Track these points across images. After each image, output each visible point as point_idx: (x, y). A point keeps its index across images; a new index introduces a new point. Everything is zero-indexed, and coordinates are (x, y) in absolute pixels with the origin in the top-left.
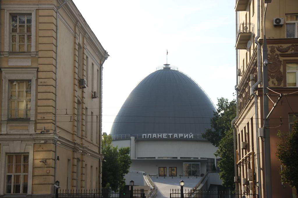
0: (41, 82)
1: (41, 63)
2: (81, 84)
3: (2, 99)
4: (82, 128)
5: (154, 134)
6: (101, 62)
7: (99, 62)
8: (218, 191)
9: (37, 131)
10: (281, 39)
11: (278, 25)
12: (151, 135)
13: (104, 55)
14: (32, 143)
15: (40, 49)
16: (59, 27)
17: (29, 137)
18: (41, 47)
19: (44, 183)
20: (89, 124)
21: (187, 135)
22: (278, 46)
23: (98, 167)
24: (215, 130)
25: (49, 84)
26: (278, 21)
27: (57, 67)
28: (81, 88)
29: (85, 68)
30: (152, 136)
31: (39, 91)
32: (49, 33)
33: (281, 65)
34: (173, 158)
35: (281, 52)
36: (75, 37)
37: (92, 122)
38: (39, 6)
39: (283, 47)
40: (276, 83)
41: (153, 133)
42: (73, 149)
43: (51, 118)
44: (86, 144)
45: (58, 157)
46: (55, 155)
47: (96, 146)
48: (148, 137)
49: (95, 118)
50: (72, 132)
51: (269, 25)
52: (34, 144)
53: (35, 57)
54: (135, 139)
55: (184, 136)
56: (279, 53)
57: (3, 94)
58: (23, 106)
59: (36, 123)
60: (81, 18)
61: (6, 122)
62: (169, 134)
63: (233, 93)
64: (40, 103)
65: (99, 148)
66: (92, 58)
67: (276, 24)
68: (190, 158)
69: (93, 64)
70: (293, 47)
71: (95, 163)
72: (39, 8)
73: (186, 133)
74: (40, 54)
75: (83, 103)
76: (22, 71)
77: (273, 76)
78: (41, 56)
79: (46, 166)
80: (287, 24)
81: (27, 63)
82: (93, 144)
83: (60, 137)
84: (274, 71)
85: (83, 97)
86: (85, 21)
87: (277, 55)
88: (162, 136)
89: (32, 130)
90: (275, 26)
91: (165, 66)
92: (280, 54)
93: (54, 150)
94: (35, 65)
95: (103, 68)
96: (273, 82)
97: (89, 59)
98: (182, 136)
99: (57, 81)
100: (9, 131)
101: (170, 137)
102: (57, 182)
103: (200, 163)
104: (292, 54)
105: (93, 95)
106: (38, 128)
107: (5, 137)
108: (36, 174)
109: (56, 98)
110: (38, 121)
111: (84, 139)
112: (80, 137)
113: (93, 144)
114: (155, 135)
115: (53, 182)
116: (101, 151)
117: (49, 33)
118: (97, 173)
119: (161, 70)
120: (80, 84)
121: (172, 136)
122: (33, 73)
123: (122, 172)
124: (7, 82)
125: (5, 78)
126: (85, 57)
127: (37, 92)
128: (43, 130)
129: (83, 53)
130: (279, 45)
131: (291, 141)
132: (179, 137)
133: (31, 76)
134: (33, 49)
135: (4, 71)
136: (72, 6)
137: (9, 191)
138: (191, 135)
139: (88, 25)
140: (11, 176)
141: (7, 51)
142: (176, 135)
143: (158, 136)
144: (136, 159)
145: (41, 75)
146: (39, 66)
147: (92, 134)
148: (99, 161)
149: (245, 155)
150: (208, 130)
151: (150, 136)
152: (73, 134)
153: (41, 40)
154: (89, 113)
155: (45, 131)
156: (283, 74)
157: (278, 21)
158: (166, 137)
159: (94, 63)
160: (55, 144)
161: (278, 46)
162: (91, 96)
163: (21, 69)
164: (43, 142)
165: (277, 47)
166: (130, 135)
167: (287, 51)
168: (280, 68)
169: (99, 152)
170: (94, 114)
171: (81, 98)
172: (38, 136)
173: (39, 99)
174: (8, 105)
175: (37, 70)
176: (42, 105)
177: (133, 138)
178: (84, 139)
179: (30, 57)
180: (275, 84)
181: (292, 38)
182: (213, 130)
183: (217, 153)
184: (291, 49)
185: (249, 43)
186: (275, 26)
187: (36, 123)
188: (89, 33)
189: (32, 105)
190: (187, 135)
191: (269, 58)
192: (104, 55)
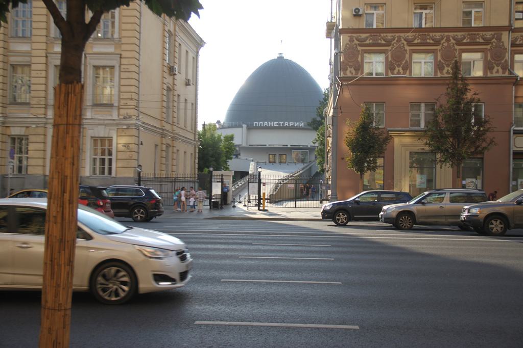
2: (171, 70)
4: (173, 114)
7: (195, 49)
9: (120, 116)
10: (486, 27)
11: (357, 15)
14: (115, 128)
15: (123, 35)
16: (142, 15)
18: (124, 34)
19: (127, 166)
20: (182, 112)
21: (298, 124)
23: (193, 153)
25: (131, 70)
26: (357, 10)
27: (141, 54)
28: (171, 75)
29: (177, 55)
31: (122, 77)
32: (132, 20)
34: (284, 145)
36: (164, 24)
37: (186, 109)
40: (354, 72)
41: (264, 121)
42: (162, 135)
43: (133, 104)
44: (177, 130)
45: (142, 142)
46: (139, 140)
47: (190, 132)
49: (189, 106)
50: (161, 119)
51: (349, 14)
52: (118, 129)
53: (118, 43)
54: (247, 126)
56: (357, 42)
58: (107, 91)
59: (119, 109)
64: (123, 89)
65: (195, 134)
68: (299, 146)
69: (187, 52)
71: (190, 149)
73: (297, 122)
74: (124, 41)
77: (351, 65)
79: (128, 150)
80: (366, 14)
81: (111, 49)
82: (187, 130)
83: (143, 123)
84: (353, 60)
87: (355, 44)
88: (273, 124)
89: (115, 116)
90: (355, 15)
91: (279, 56)
92: (359, 44)
94: (118, 52)
96: (350, 72)
99: (141, 67)
102: (140, 166)
106: (121, 114)
107: (90, 121)
108: (119, 158)
109: (139, 84)
110: (121, 107)
113: (187, 130)
114: (266, 124)
115: (137, 166)
117: (132, 20)
118: (191, 158)
119: (275, 59)
121: (282, 124)
123: (225, 158)
124: (92, 67)
125: (90, 64)
126: (177, 44)
127: (120, 78)
129: (175, 40)
131: (357, 129)
133: (115, 63)
134: (116, 36)
137: (94, 172)
138: (301, 123)
140: (96, 158)
141: (53, 36)
142: (286, 124)
143: (270, 124)
144: (248, 146)
145: (124, 61)
146: (122, 53)
147: (185, 121)
148: (195, 148)
150: (314, 119)
151: (261, 124)
152: (161, 120)
153: (124, 26)
154: (182, 99)
155: (128, 117)
159: (189, 51)
162: (184, 83)
164: (125, 127)
167: (365, 41)
169: (195, 138)
170: (188, 102)
171: (172, 84)
172: (121, 122)
173: (122, 86)
174: (93, 91)
175: (119, 56)
177: (245, 126)
179: (113, 43)
180: (352, 74)
181: (371, 28)
183: (315, 141)
184: (369, 39)
186: (355, 15)
187: (119, 109)
189: (115, 91)
190: (298, 124)
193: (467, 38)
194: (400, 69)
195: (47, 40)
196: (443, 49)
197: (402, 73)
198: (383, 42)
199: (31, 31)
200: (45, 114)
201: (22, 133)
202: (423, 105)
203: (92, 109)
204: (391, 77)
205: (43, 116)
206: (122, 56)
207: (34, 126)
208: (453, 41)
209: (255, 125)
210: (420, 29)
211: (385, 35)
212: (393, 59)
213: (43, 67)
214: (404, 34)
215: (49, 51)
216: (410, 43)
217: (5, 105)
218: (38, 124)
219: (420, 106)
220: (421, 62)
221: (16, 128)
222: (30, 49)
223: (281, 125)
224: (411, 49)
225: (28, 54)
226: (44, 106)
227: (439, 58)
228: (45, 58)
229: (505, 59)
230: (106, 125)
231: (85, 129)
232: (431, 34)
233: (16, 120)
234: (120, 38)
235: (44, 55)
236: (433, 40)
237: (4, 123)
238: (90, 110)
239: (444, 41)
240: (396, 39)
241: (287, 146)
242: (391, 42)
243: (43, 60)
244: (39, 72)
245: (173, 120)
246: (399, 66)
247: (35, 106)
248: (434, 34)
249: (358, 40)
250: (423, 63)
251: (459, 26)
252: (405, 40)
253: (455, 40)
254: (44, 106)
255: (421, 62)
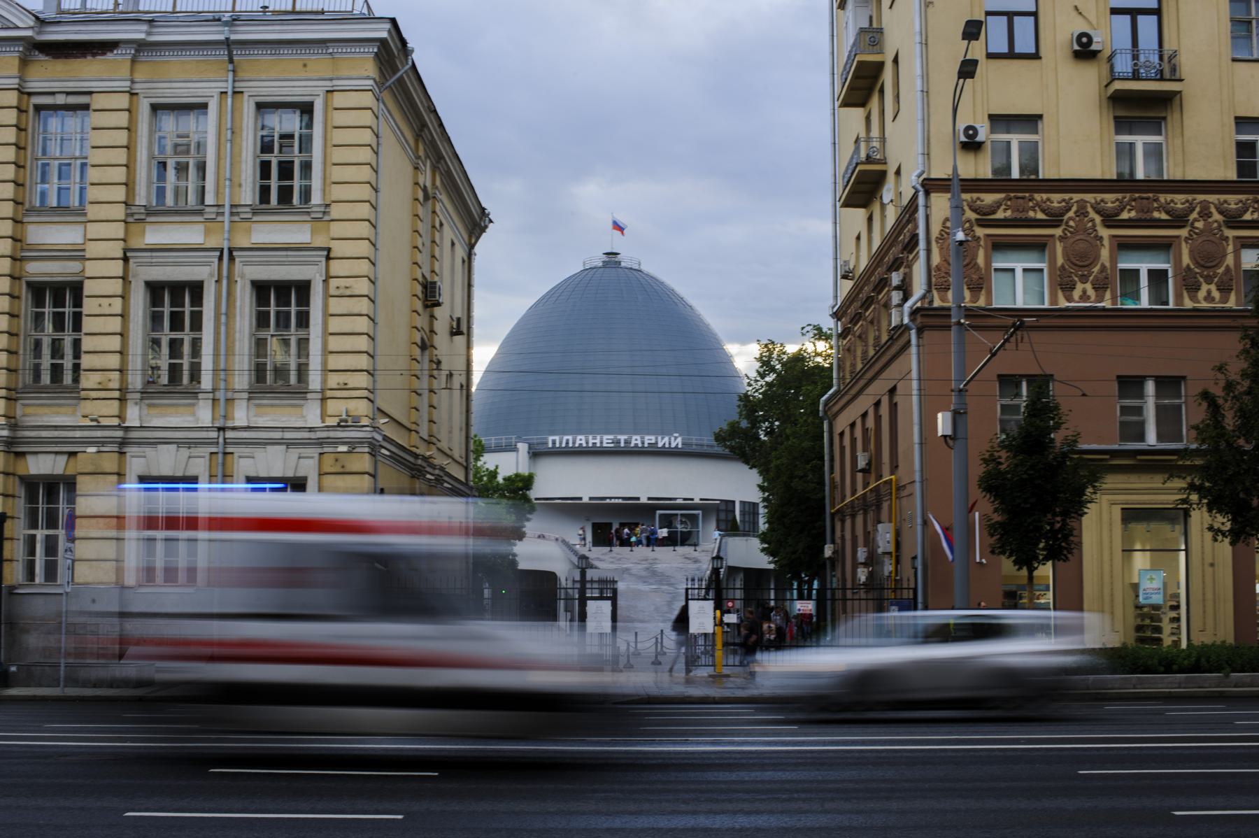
0: (338, 288)
1: (336, 236)
3: (235, 332)
5: (579, 437)
6: (470, 237)
8: (746, 589)
12: (570, 438)
13: (481, 219)
14: (314, 452)
17: (306, 435)
18: (338, 192)
21: (666, 439)
22: (971, 198)
24: (749, 425)
26: (971, 131)
30: (574, 443)
31: (332, 310)
33: (978, 249)
34: (685, 499)
35: (978, 214)
38: (335, 82)
39: (982, 201)
48: (564, 445)
52: (321, 454)
54: (530, 448)
55: (657, 443)
56: (972, 216)
57: (238, 318)
60: (432, 116)
61: (246, 395)
62: (619, 437)
63: (803, 328)
66: (451, 227)
67: (966, 140)
68: (675, 499)
69: (453, 244)
70: (1009, 203)
72: (333, 86)
74: (336, 211)
75: (433, 346)
76: (152, 257)
78: (92, 219)
85: (432, 331)
86: (441, 125)
87: (969, 221)
92: (977, 220)
93: (371, 471)
94: (320, 241)
95: (475, 254)
97: (446, 226)
98: (653, 441)
100: (255, 419)
101: (622, 445)
103: (700, 512)
104: (1005, 220)
105: (455, 327)
106: (329, 412)
110: (329, 394)
111: (434, 444)
112: (426, 437)
114: (581, 440)
116: (471, 477)
120: (426, 296)
122: (315, 264)
125: (242, 276)
127: (327, 315)
128: (344, 417)
130: (975, 195)
132: (646, 445)
133: (310, 272)
134: (316, 198)
135: (240, 256)
136: (415, 83)
138: (676, 438)
139: (449, 138)
142: (636, 440)
145: (337, 267)
146: (333, 244)
149: (864, 489)
151: (568, 440)
156: (983, 272)
157: (971, 132)
158: (612, 445)
159: (456, 241)
160: (373, 454)
161: (1095, 198)
163: (148, 254)
165: (970, 200)
166: (516, 438)
167: (994, 212)
168: (977, 256)
171: (427, 332)
175: (325, 253)
176: (339, 350)
177: (523, 447)
178: (434, 444)
179: (307, 218)
181: (1033, 177)
182: (744, 424)
184: (1003, 207)
185: (887, 190)
188: (449, 157)
190: (666, 439)
191: (1071, 227)
192: (481, 219)
193: (1251, 209)
194: (1088, 286)
195: (127, 215)
196: (1195, 236)
197: (1093, 298)
198: (1040, 216)
199: (82, 190)
200: (121, 417)
201: (59, 470)
202: (1150, 387)
203: (249, 399)
204: (1067, 309)
205: (115, 422)
206: (332, 255)
207: (92, 450)
208: (1217, 216)
209: (550, 445)
210: (1124, 183)
211: (1045, 196)
212: (1069, 260)
213: (116, 287)
214: (1217, 196)
215: (134, 243)
216: (1111, 220)
217: (13, 394)
218: (103, 444)
219: (1018, 385)
220: (1013, 270)
221: (41, 457)
222: (80, 241)
223: (622, 444)
224: (1238, 238)
225: (77, 254)
226: (116, 394)
227: (1186, 260)
228: (121, 262)
229: (1225, 265)
230: (289, 444)
231: (229, 457)
232: (1163, 198)
233: (44, 434)
234: (327, 206)
235: (120, 254)
236: (1167, 213)
237: (10, 443)
238: (244, 403)
239: (1194, 215)
240: (1074, 209)
241: (692, 499)
242: (1062, 215)
243: (117, 268)
244: (105, 301)
245: (430, 430)
246: (1084, 279)
247: (94, 394)
248: (1169, 197)
249: (975, 210)
250: (1019, 274)
251: (1107, 177)
252: (1098, 212)
253: (1221, 213)
254: (116, 394)
255: (1013, 270)
